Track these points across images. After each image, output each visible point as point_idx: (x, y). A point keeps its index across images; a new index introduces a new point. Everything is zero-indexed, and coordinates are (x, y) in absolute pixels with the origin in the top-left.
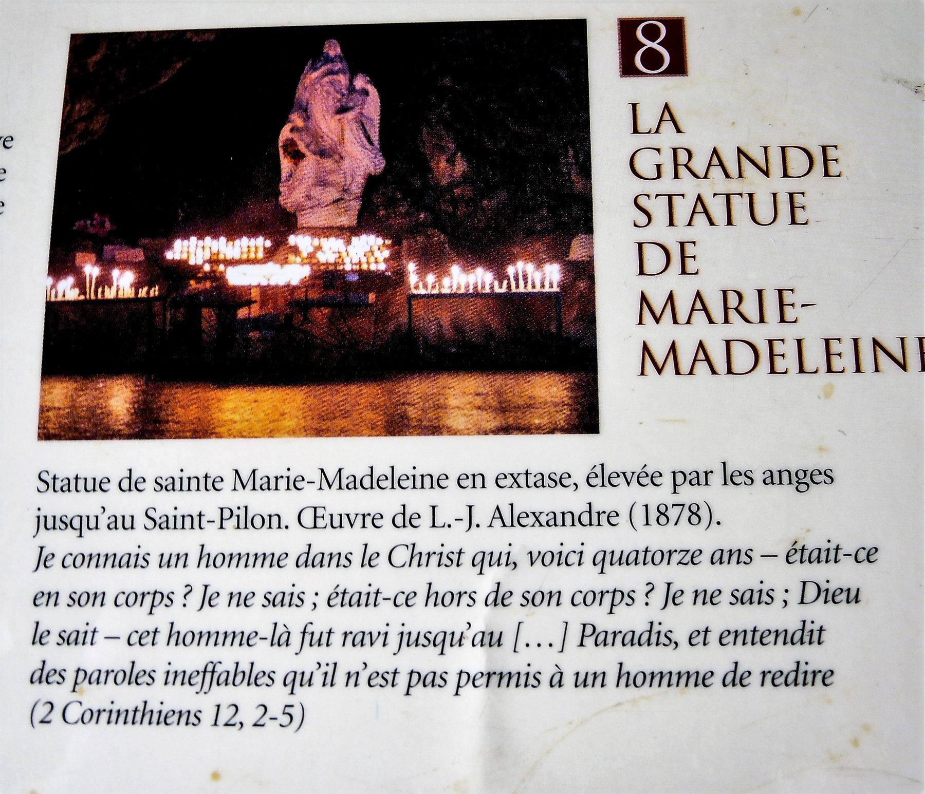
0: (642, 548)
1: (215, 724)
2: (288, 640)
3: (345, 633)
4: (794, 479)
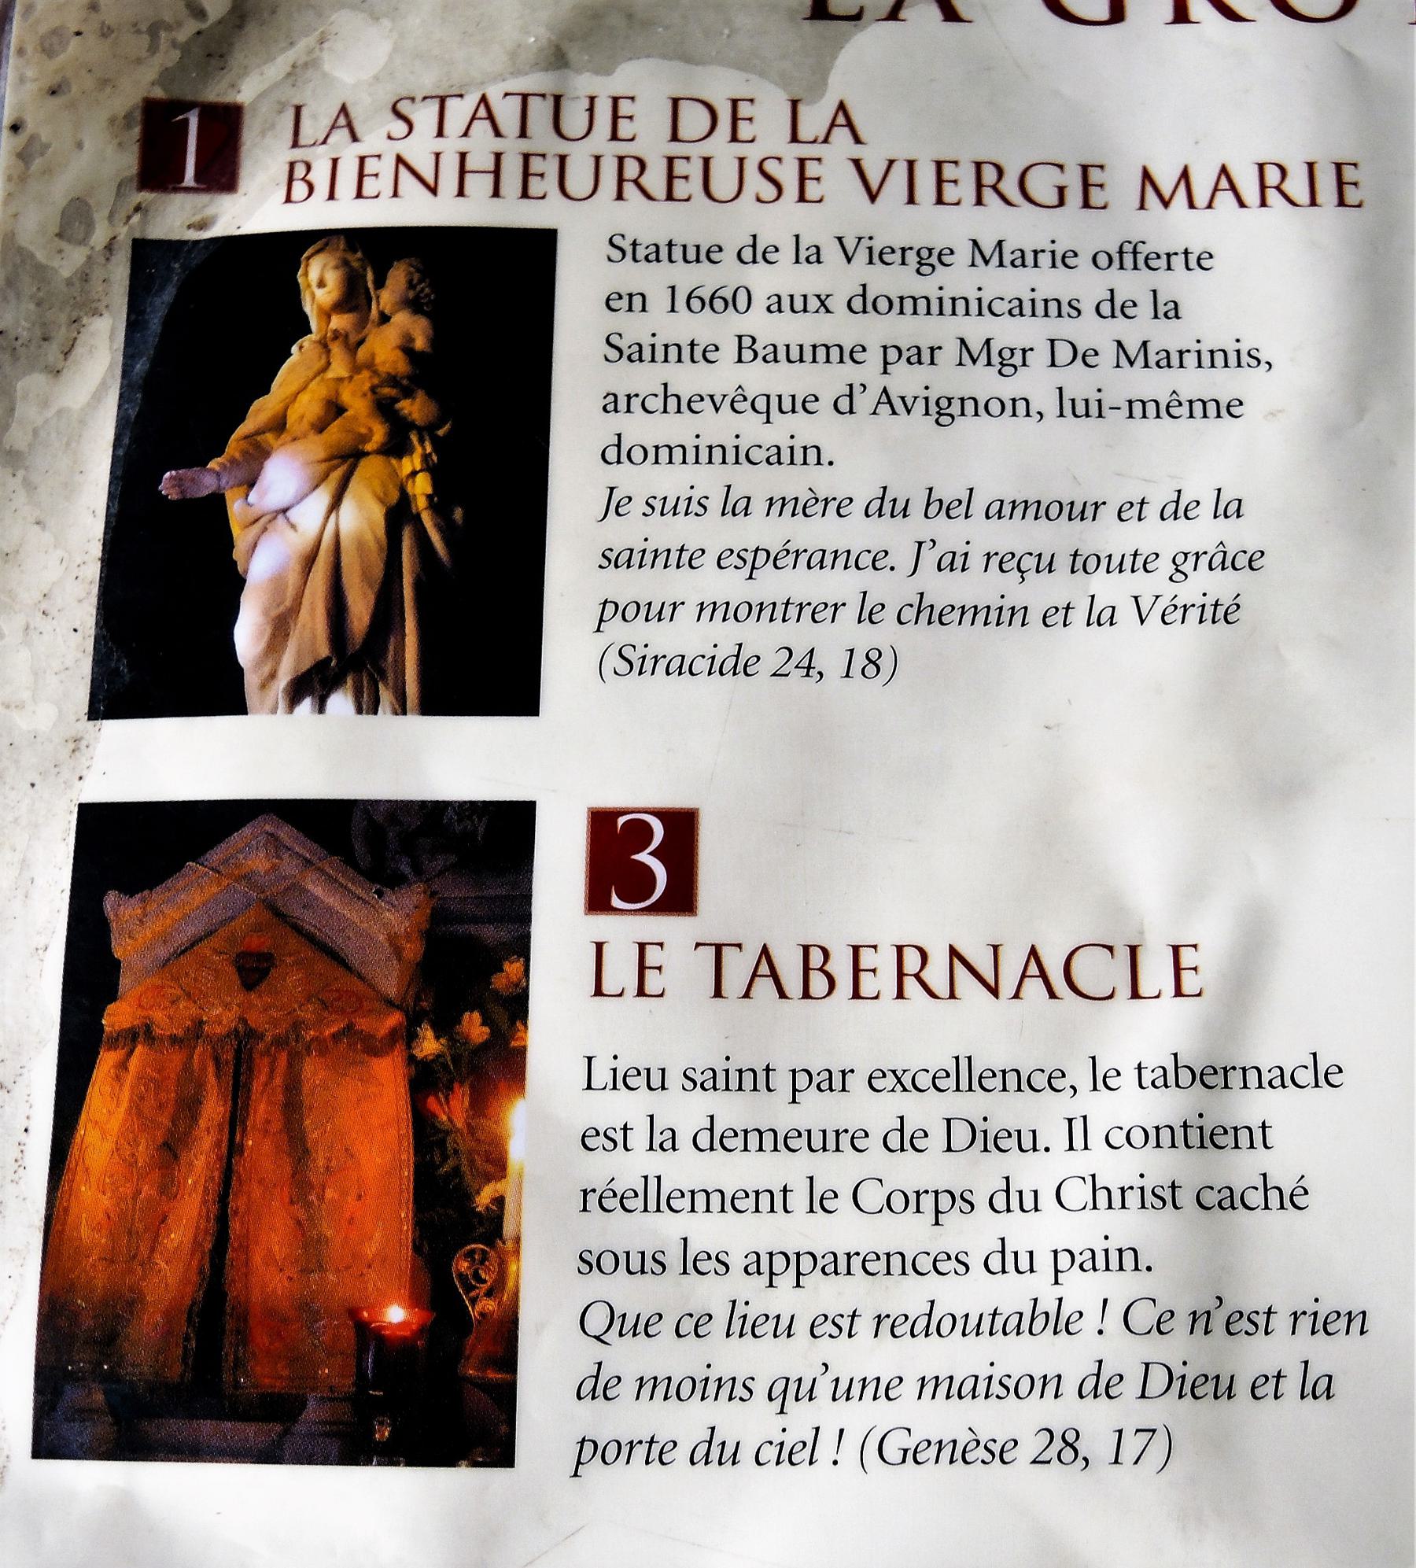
0: (675, 547)
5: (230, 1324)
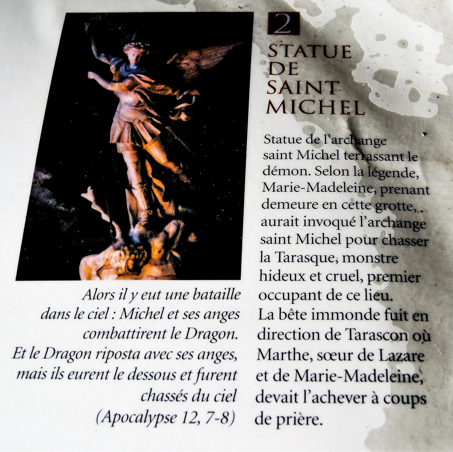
0: (209, 292)
1: (184, 422)
2: (138, 356)
3: (98, 352)
4: (68, 356)
5: (149, 90)
